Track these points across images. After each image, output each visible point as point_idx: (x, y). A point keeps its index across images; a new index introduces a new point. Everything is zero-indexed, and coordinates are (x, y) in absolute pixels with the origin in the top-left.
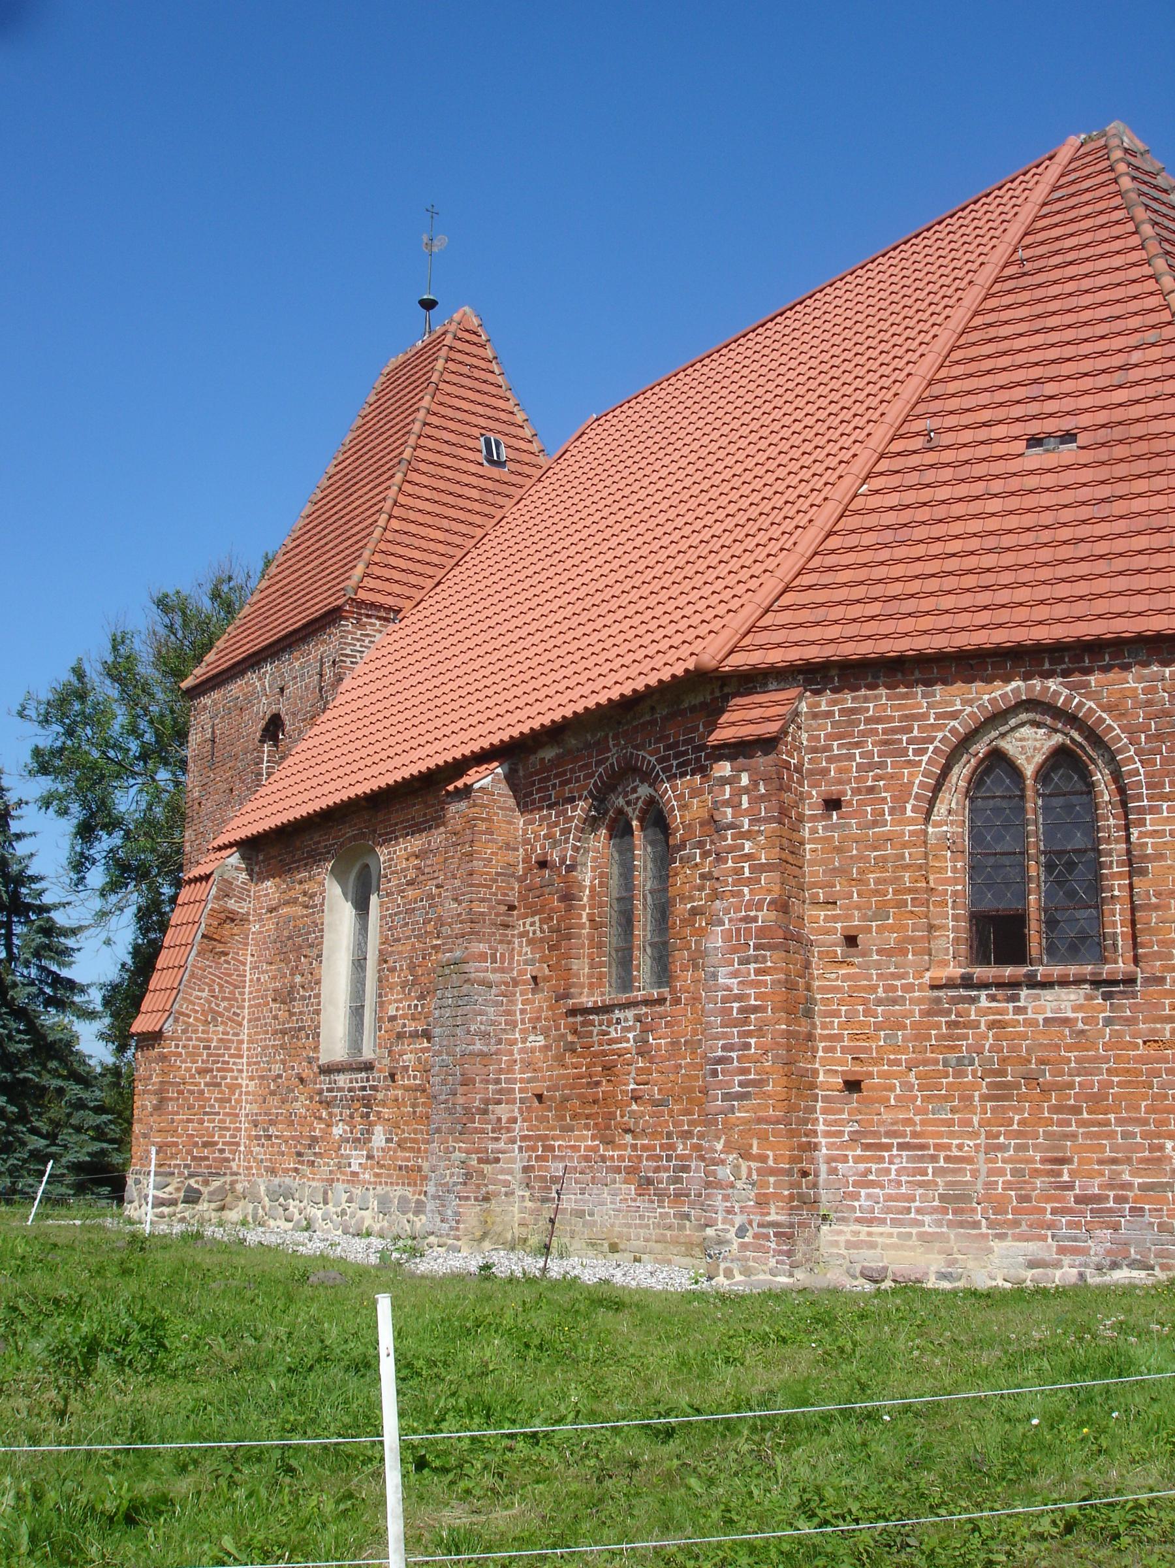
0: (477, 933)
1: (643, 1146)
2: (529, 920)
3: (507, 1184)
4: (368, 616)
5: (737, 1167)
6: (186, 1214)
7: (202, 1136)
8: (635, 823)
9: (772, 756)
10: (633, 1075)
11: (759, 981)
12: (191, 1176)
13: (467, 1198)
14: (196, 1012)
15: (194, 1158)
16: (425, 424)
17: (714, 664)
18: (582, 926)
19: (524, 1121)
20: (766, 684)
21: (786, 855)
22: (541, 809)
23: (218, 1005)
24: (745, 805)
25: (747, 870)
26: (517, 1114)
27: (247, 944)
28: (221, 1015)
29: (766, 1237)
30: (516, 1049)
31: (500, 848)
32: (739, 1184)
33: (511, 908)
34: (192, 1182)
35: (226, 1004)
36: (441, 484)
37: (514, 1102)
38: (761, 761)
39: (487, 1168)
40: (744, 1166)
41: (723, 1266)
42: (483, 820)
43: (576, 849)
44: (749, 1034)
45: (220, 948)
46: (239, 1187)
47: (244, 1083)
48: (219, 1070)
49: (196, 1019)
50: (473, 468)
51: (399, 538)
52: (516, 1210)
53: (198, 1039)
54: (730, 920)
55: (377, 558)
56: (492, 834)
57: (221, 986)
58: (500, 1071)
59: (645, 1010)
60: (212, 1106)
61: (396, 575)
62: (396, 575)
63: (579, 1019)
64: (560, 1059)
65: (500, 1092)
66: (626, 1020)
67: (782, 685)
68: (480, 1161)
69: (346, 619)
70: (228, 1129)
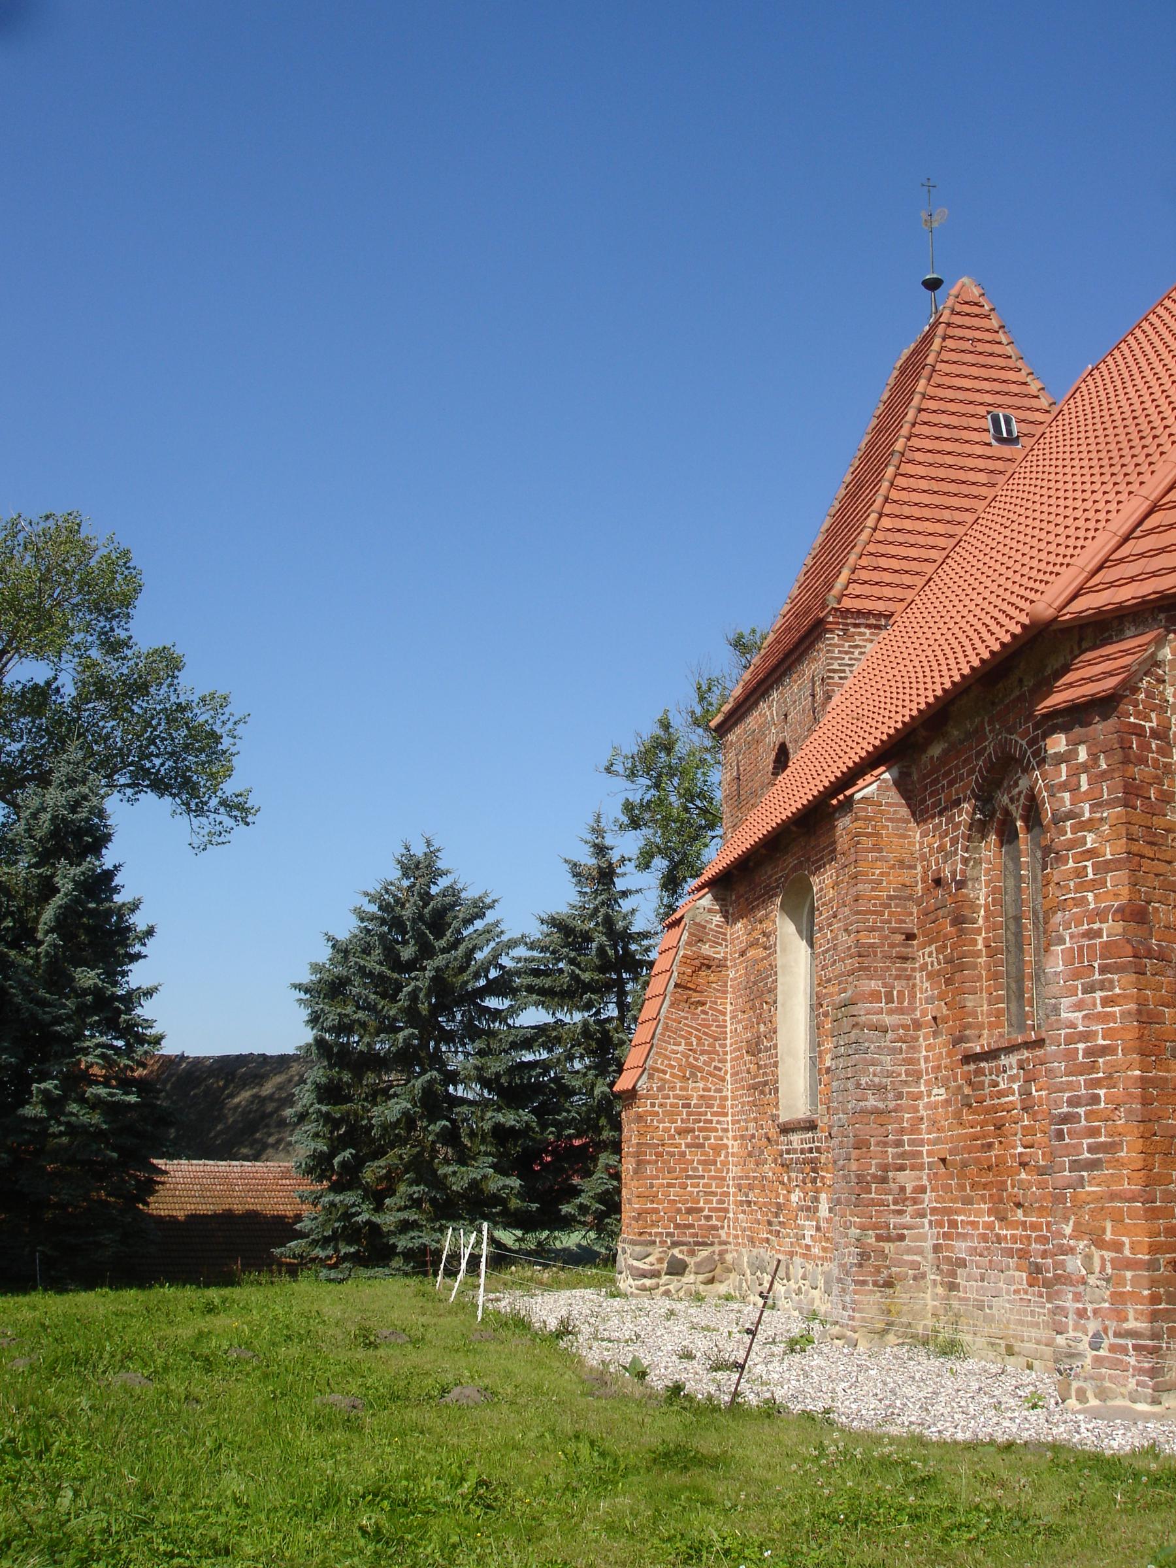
0: (867, 969)
1: (1032, 1223)
2: (928, 950)
3: (915, 1266)
4: (856, 626)
5: (1088, 1258)
6: (671, 1287)
7: (687, 1201)
8: (1019, 823)
9: (1113, 720)
10: (1019, 1136)
11: (1107, 1014)
12: (675, 1244)
13: (864, 1283)
14: (673, 1067)
15: (677, 1226)
16: (920, 410)
17: (1050, 612)
18: (978, 954)
19: (932, 1191)
20: (1122, 631)
21: (1140, 846)
22: (933, 817)
23: (696, 1059)
24: (1084, 787)
25: (1090, 870)
26: (925, 1182)
27: (726, 992)
28: (700, 1070)
29: (1124, 1350)
30: (921, 1103)
31: (892, 867)
32: (1092, 1280)
33: (910, 937)
34: (676, 1251)
35: (705, 1057)
36: (941, 473)
37: (921, 1167)
38: (1102, 729)
39: (888, 1247)
40: (1097, 1254)
41: (1075, 1385)
42: (868, 835)
43: (965, 861)
44: (1097, 1083)
45: (696, 997)
46: (729, 1257)
47: (730, 1143)
48: (701, 1130)
49: (673, 1075)
50: (979, 450)
51: (890, 537)
52: (928, 1296)
53: (677, 1097)
54: (1071, 938)
55: (864, 562)
56: (880, 851)
57: (699, 1039)
58: (902, 1131)
59: (1026, 1054)
60: (695, 1169)
61: (887, 577)
62: (887, 577)
63: (972, 1067)
64: (958, 1115)
65: (902, 1155)
66: (1011, 1068)
67: (1140, 630)
68: (879, 1238)
69: (831, 631)
70: (714, 1194)
